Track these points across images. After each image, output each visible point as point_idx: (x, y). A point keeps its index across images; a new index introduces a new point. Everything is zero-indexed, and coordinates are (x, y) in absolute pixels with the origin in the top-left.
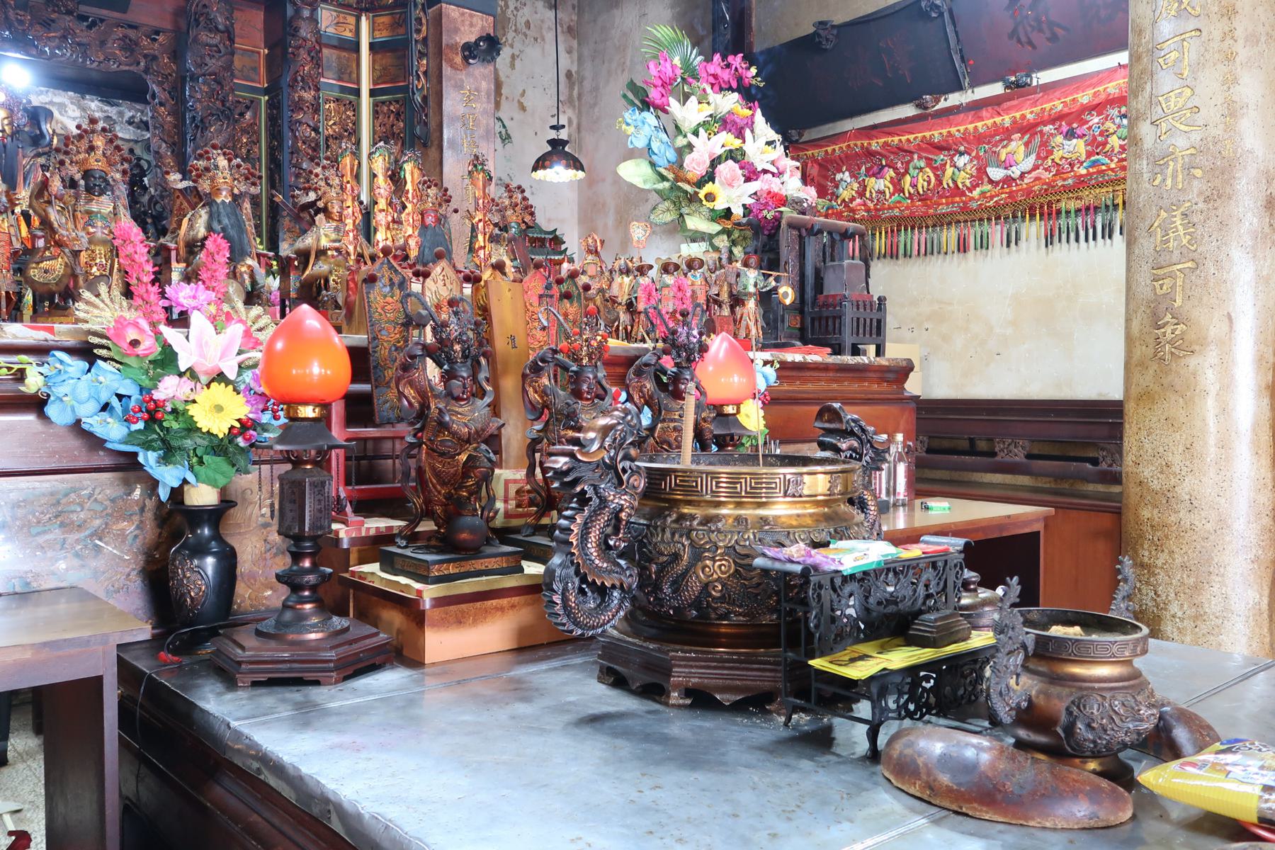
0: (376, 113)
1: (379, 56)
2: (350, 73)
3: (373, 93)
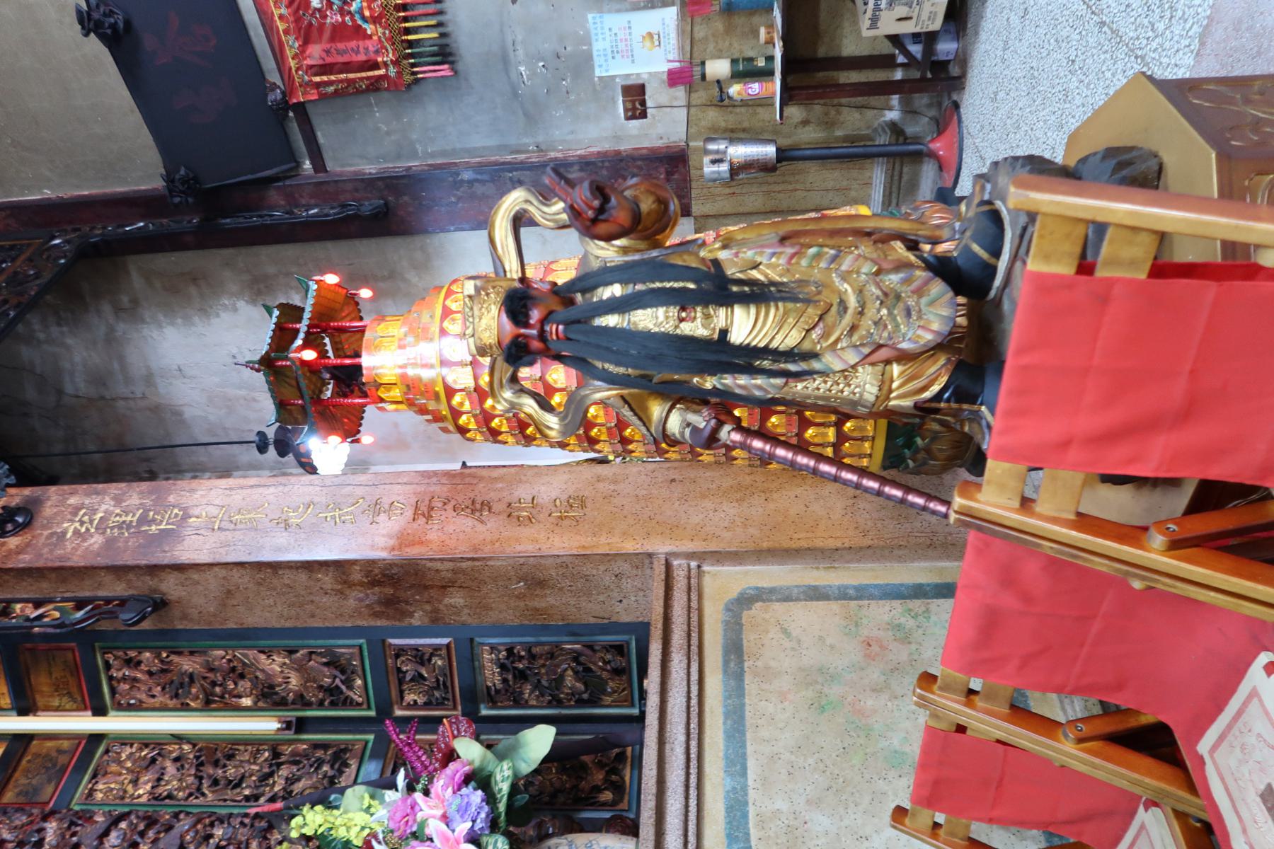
0: (138, 707)
1: (41, 701)
2: (60, 751)
3: (100, 711)
